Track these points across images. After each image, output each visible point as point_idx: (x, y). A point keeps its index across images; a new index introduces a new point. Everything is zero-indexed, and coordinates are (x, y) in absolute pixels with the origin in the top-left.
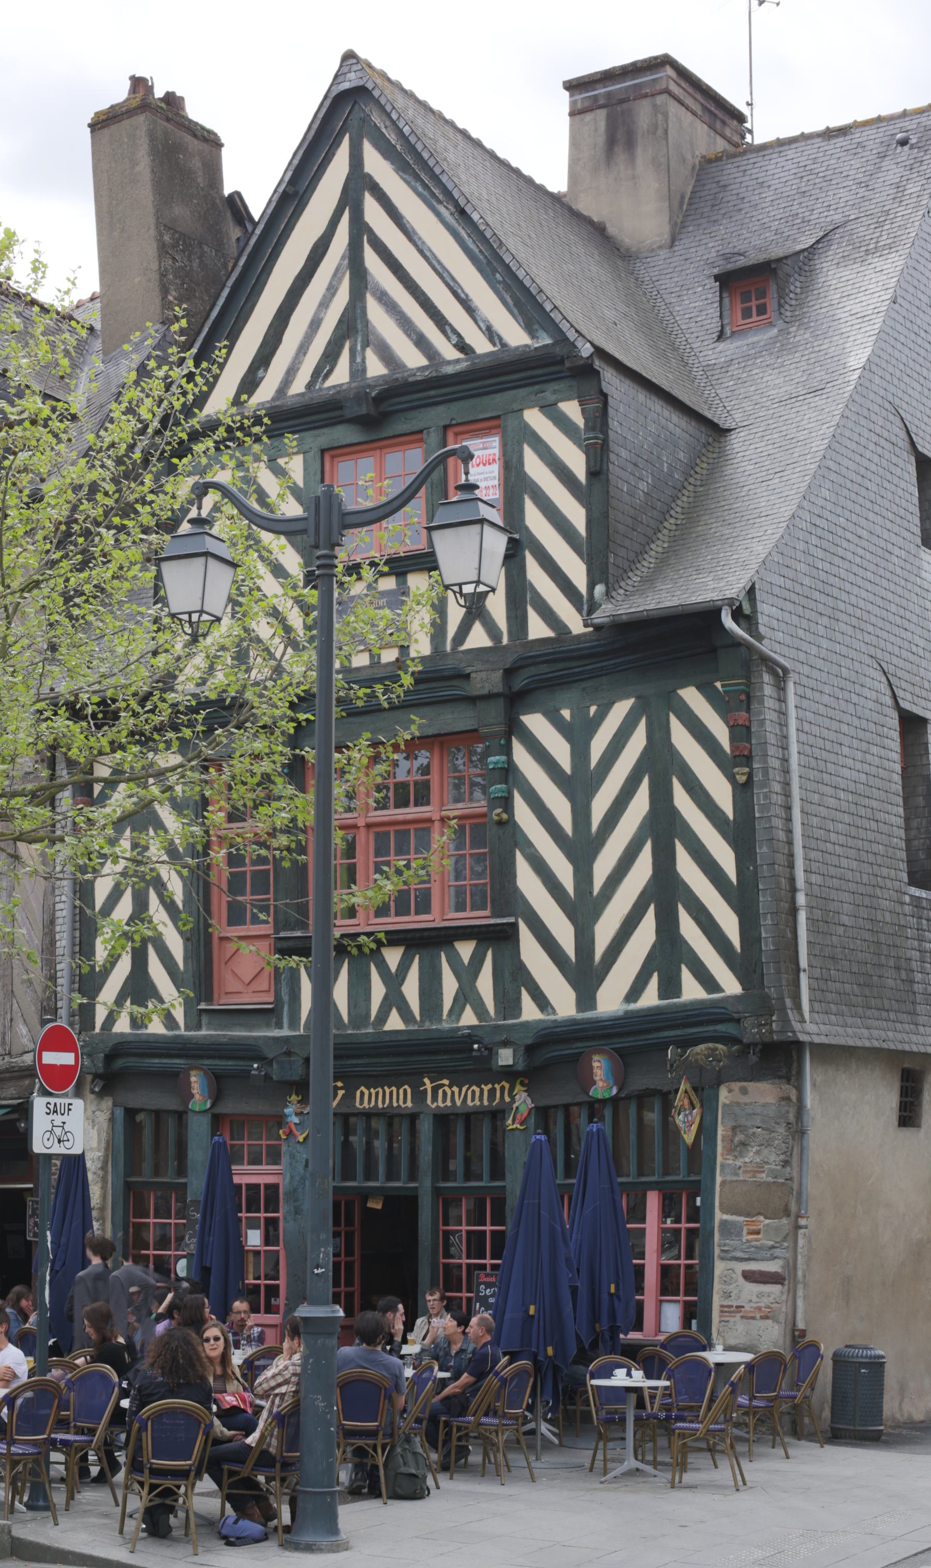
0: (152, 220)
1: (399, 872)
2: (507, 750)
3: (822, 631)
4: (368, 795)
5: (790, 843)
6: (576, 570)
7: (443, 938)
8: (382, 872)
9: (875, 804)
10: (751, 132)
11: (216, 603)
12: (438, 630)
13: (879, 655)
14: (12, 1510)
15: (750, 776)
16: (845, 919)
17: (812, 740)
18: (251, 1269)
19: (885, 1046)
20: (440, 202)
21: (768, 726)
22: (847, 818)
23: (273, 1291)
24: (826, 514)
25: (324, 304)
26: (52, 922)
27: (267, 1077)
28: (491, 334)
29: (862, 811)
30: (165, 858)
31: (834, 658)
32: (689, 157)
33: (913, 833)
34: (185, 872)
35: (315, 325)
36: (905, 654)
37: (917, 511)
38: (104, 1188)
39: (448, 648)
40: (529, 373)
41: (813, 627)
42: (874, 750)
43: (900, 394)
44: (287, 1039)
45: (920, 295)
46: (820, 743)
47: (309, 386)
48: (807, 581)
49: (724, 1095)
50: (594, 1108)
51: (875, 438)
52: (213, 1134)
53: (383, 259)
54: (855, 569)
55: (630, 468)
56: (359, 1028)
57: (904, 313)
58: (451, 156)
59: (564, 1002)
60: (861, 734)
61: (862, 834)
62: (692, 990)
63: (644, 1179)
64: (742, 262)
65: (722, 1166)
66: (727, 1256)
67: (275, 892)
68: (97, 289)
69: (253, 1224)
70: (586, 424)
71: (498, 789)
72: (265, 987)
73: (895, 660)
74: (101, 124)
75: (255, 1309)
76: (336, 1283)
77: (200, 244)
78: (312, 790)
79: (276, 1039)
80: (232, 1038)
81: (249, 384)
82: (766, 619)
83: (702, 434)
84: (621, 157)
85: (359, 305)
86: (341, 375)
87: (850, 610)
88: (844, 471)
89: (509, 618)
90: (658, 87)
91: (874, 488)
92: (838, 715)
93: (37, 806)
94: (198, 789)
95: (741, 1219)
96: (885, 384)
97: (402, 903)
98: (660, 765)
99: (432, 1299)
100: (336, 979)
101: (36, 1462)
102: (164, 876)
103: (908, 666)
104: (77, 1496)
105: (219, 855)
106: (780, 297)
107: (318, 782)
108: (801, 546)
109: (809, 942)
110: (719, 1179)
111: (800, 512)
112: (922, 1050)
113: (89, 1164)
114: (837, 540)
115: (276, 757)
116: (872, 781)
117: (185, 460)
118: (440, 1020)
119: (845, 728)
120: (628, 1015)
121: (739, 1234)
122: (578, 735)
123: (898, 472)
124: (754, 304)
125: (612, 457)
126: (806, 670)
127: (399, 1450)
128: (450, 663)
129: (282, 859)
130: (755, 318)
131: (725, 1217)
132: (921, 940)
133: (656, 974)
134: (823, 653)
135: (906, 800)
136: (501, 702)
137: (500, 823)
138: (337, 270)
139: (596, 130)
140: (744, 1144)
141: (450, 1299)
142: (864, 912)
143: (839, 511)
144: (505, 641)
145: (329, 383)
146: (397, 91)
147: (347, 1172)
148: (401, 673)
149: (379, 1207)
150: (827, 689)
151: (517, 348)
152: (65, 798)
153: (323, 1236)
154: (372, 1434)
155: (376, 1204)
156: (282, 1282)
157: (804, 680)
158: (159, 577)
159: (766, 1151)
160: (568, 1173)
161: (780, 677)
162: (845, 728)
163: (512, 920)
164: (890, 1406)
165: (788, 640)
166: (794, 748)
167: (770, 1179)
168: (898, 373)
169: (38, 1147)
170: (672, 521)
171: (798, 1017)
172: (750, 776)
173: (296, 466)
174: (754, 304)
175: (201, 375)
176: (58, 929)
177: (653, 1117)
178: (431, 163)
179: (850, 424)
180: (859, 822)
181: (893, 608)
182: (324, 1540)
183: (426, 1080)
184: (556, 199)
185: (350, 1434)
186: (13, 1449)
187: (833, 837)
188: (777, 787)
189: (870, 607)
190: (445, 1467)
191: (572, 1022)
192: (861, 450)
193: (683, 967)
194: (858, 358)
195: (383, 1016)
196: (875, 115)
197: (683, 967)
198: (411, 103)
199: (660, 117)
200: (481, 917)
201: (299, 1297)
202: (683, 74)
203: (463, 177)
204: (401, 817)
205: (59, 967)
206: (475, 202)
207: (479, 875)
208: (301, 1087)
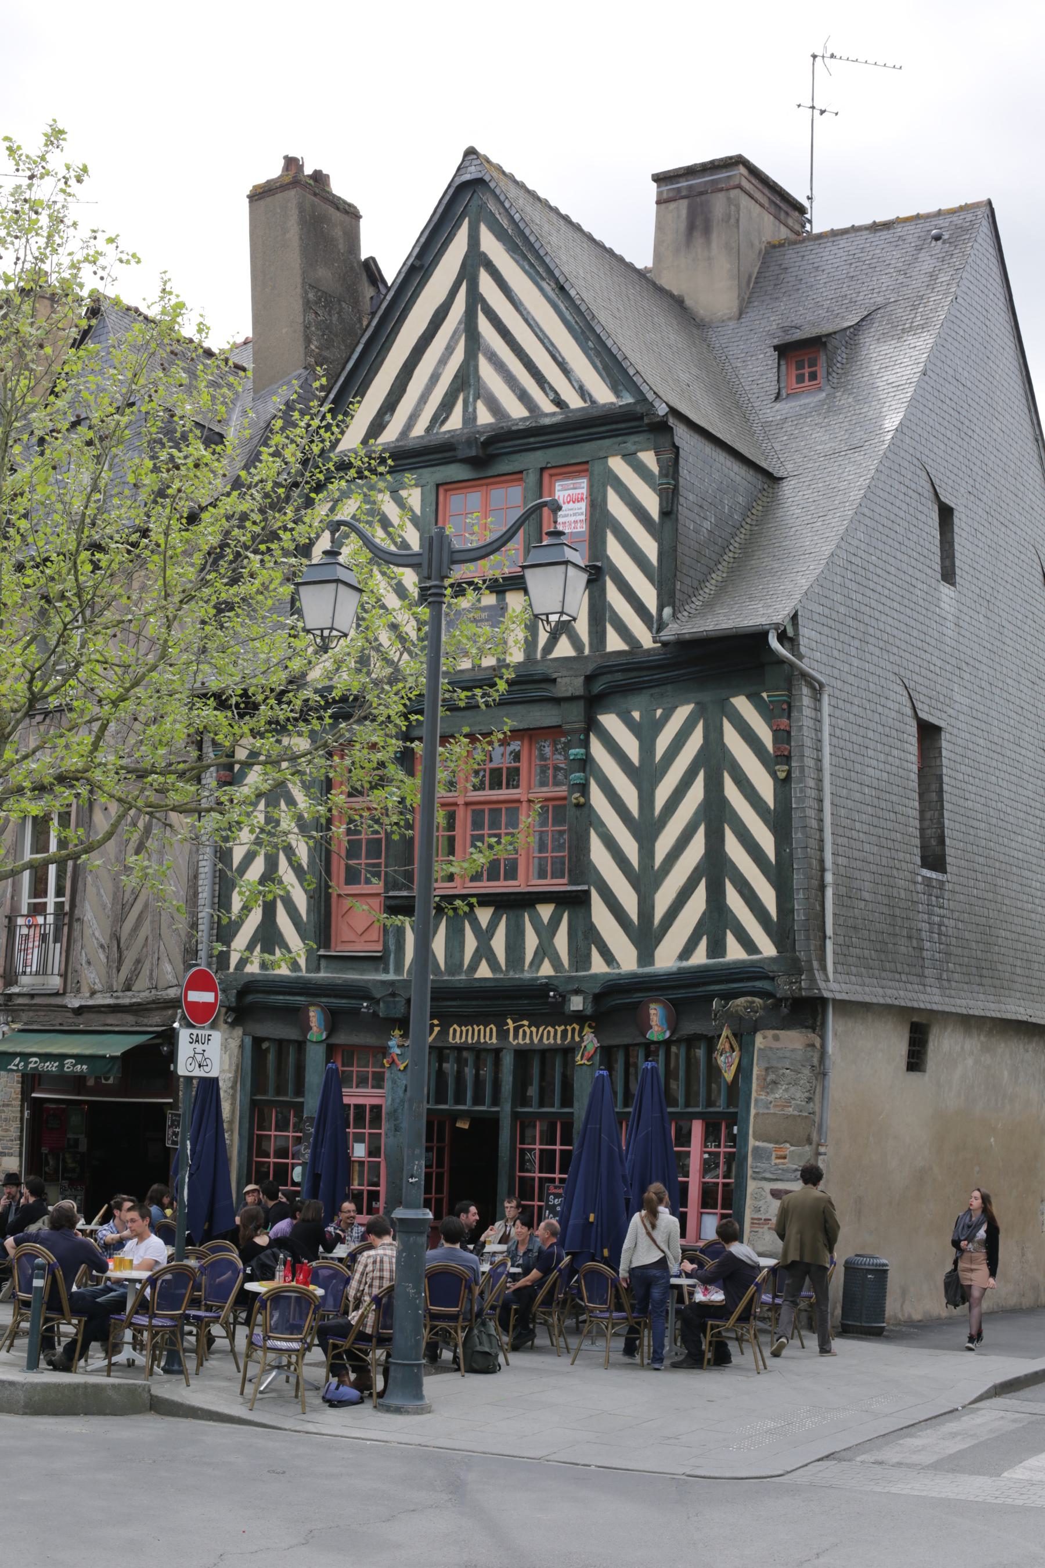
0: (299, 280)
1: (491, 847)
2: (586, 744)
3: (853, 651)
4: (467, 780)
5: (821, 830)
6: (648, 595)
7: (527, 901)
8: (476, 847)
9: (894, 798)
10: (810, 221)
11: (345, 620)
12: (530, 644)
13: (902, 672)
14: (151, 1373)
15: (789, 773)
16: (866, 895)
17: (842, 743)
18: (356, 1177)
19: (896, 1003)
20: (543, 279)
21: (805, 732)
22: (870, 810)
23: (374, 1196)
24: (861, 553)
25: (443, 361)
26: (196, 877)
27: (375, 1014)
28: (583, 392)
29: (883, 805)
30: (296, 830)
31: (863, 674)
32: (756, 242)
33: (927, 823)
34: (311, 843)
35: (434, 378)
36: (924, 672)
37: (938, 551)
38: (233, 1104)
39: (539, 656)
40: (614, 427)
41: (846, 648)
42: (895, 752)
43: (927, 452)
44: (392, 983)
45: (947, 368)
46: (849, 746)
47: (428, 430)
48: (842, 609)
49: (760, 1040)
50: (650, 1049)
51: (904, 489)
52: (328, 1061)
53: (494, 326)
54: (884, 600)
55: (696, 509)
56: (453, 975)
57: (933, 383)
58: (554, 239)
59: (627, 959)
60: (885, 739)
61: (883, 823)
62: (735, 952)
63: (690, 1110)
64: (798, 335)
65: (756, 1100)
66: (758, 1177)
67: (387, 857)
68: (250, 335)
69: (360, 1139)
70: (660, 471)
71: (577, 777)
72: (375, 938)
73: (915, 677)
74: (259, 195)
75: (359, 1211)
76: (427, 1190)
77: (339, 301)
78: (419, 775)
79: (383, 983)
80: (346, 980)
81: (377, 427)
82: (806, 641)
83: (758, 481)
84: (699, 239)
85: (472, 363)
86: (455, 422)
87: (878, 634)
88: (877, 517)
89: (590, 633)
90: (732, 183)
91: (903, 531)
92: (866, 723)
93: (187, 781)
94: (323, 771)
95: (771, 1145)
96: (914, 444)
97: (493, 871)
98: (714, 762)
99: (510, 1207)
100: (435, 933)
101: (173, 1333)
102: (294, 844)
103: (927, 683)
104: (205, 1363)
105: (339, 830)
106: (828, 366)
107: (425, 768)
108: (838, 580)
109: (835, 914)
110: (753, 1112)
111: (838, 551)
112: (929, 1007)
113: (221, 1084)
114: (869, 575)
115: (390, 749)
116: (892, 779)
117: (321, 496)
118: (522, 970)
119: (870, 734)
120: (681, 972)
121: (769, 1158)
122: (646, 734)
123: (923, 518)
124: (806, 371)
125: (682, 500)
126: (839, 684)
127: (476, 1332)
128: (540, 669)
129: (393, 832)
130: (807, 383)
131: (757, 1144)
132: (930, 914)
133: (705, 938)
134: (854, 670)
135: (921, 795)
136: (582, 703)
137: (578, 806)
138: (455, 332)
139: (679, 217)
140: (775, 1083)
141: (524, 1207)
142: (882, 890)
143: (872, 550)
144: (587, 652)
145: (446, 428)
146: (510, 183)
147: (440, 1096)
148: (497, 680)
149: (466, 1127)
150: (856, 701)
151: (604, 405)
152: (210, 779)
153: (417, 1151)
154: (454, 1318)
155: (463, 1125)
156: (382, 1189)
157: (837, 693)
158: (297, 592)
159: (793, 1089)
160: (626, 1104)
161: (817, 690)
162: (870, 734)
163: (585, 887)
164: (893, 1307)
165: (825, 659)
166: (827, 750)
167: (796, 1113)
168: (926, 435)
169: (182, 1071)
170: (731, 554)
171: (823, 977)
172: (789, 773)
173: (414, 497)
174: (806, 371)
175: (338, 426)
176: (200, 882)
177: (700, 1053)
178: (537, 246)
179: (883, 478)
180: (880, 813)
181: (915, 633)
182: (411, 1404)
183: (509, 1021)
184: (641, 274)
185: (434, 1317)
186: (154, 1322)
187: (858, 825)
188: (811, 783)
189: (895, 632)
190: (516, 1348)
191: (634, 975)
192: (891, 499)
193: (728, 932)
194: (892, 421)
195: (474, 966)
196: (914, 213)
197: (728, 932)
198: (521, 193)
199: (733, 208)
200: (560, 885)
201: (396, 1201)
202: (754, 172)
203: (564, 258)
204: (495, 798)
205: (200, 915)
206: (573, 280)
207: (560, 847)
208: (403, 1023)
